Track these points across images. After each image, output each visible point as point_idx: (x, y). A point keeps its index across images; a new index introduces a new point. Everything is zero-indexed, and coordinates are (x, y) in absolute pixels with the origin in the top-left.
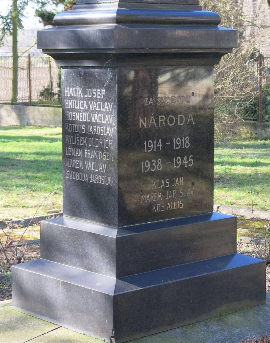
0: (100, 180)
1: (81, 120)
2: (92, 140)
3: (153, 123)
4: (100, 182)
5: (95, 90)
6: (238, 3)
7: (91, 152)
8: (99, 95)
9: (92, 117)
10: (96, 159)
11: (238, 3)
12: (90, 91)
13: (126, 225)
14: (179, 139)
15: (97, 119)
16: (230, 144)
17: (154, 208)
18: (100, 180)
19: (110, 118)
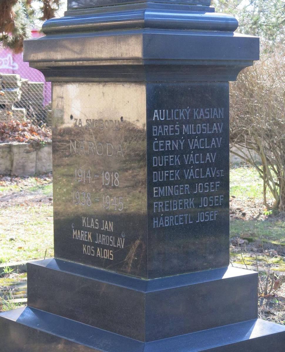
0: (108, 241)
1: (193, 133)
2: (174, 118)
3: (196, 145)
4: (108, 243)
5: (183, 186)
6: (7, 127)
7: (158, 128)
8: (213, 188)
9: (218, 144)
10: (101, 234)
11: (7, 127)
12: (161, 179)
13: (82, 274)
14: (107, 173)
15: (197, 145)
16: (71, 185)
17: (84, 221)
18: (108, 241)
19: (218, 141)
